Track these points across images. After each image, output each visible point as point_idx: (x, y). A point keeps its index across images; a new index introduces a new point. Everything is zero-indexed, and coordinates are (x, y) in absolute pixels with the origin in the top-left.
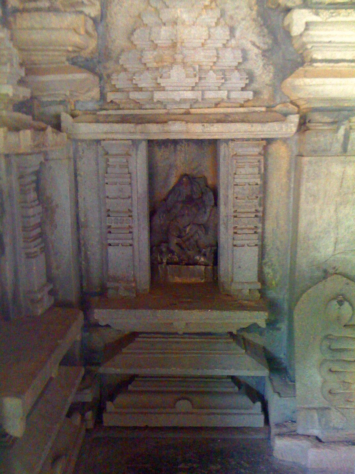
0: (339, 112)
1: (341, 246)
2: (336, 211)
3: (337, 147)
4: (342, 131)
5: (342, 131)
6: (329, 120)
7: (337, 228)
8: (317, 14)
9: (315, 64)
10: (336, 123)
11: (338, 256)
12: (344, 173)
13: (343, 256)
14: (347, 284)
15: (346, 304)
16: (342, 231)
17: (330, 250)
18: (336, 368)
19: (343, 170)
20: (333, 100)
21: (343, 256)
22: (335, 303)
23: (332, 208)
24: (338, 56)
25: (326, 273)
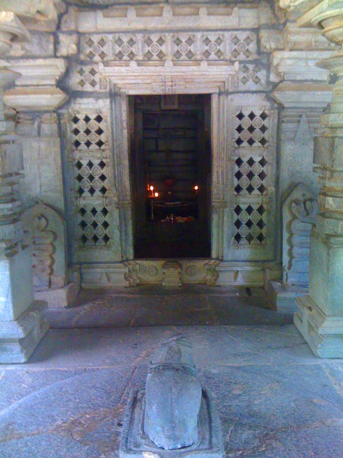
0: (341, 76)
1: (44, 188)
2: (38, 168)
3: (35, 132)
4: (36, 124)
5: (36, 124)
6: (30, 118)
7: (40, 178)
8: (8, 62)
9: (16, 88)
10: (33, 120)
11: (43, 193)
12: (40, 147)
13: (46, 194)
14: (46, 208)
15: (43, 220)
16: (43, 179)
17: (38, 190)
18: (37, 252)
19: (38, 145)
20: (27, 107)
21: (46, 194)
22: (37, 219)
23: (36, 167)
24: (29, 83)
25: (36, 202)
